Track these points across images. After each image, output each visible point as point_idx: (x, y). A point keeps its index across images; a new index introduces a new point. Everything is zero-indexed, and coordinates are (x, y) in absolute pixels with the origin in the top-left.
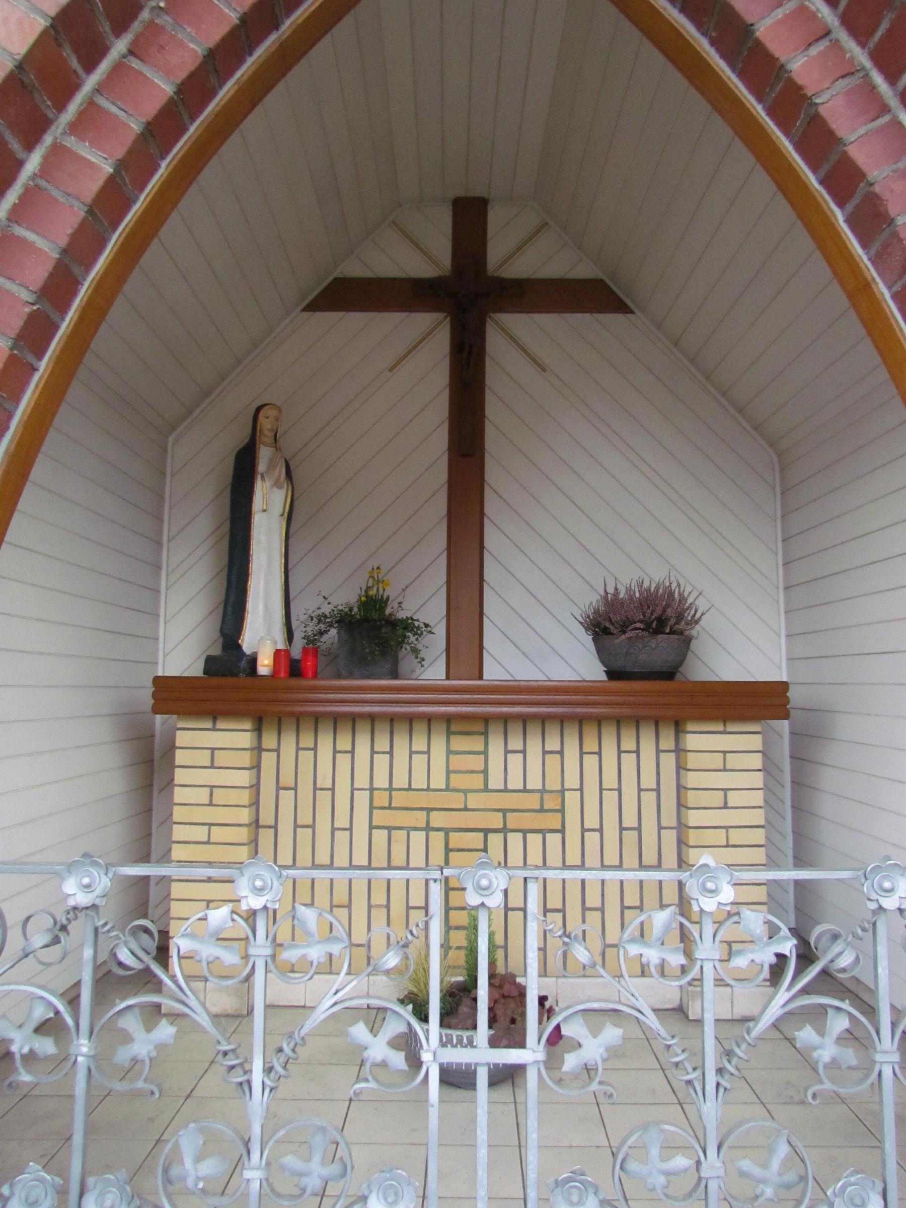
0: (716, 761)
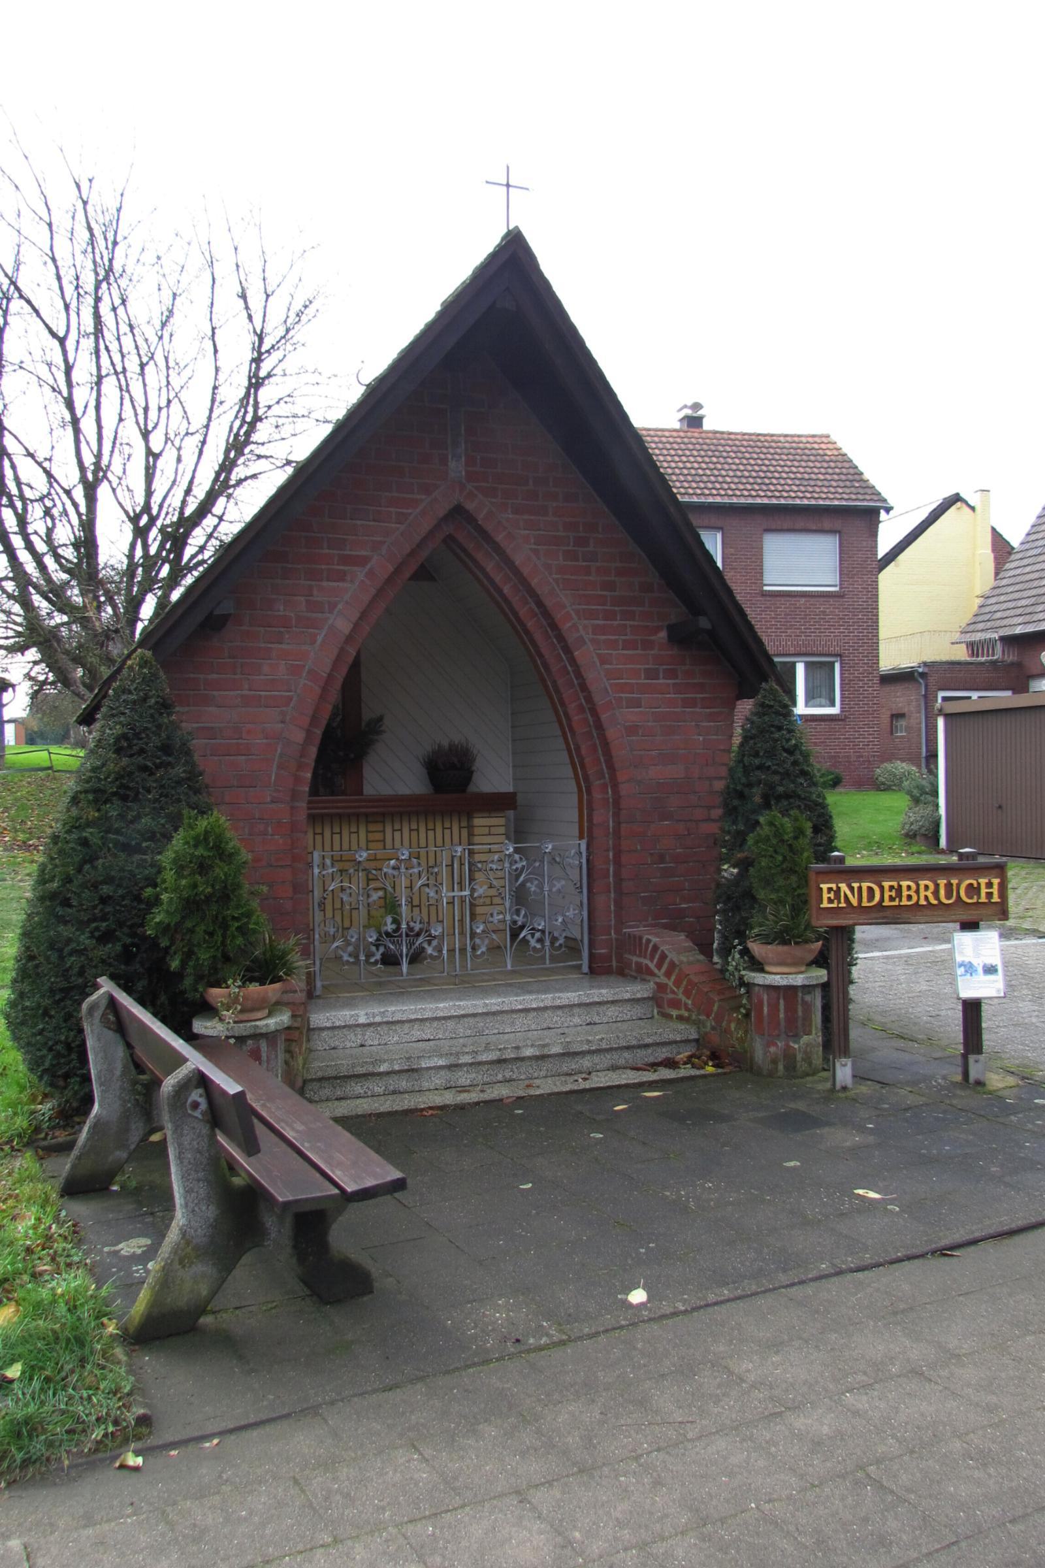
0: (486, 830)
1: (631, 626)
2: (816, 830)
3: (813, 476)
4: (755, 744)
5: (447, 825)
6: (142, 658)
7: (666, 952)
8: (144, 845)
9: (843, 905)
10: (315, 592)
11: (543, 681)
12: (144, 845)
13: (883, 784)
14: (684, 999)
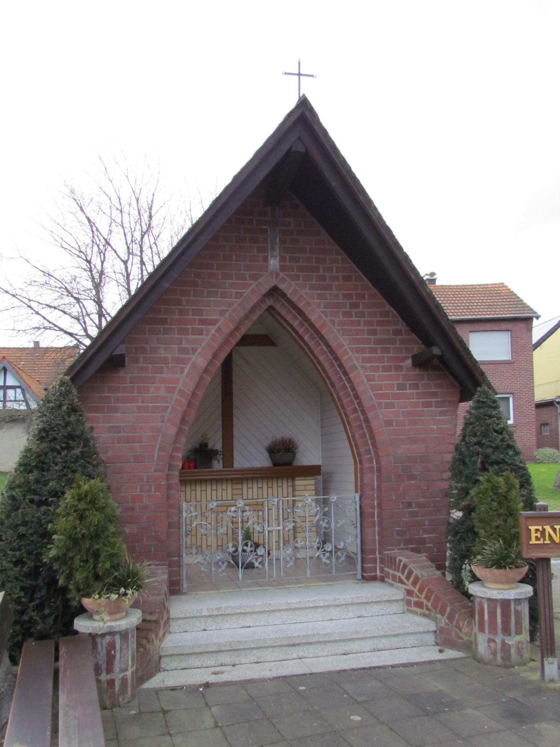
0: (303, 488)
1: (387, 357)
2: (522, 486)
3: (495, 304)
4: (474, 428)
5: (280, 484)
6: (61, 381)
7: (413, 569)
8: (50, 499)
9: (547, 542)
10: (184, 342)
11: (331, 394)
12: (50, 499)
13: (539, 460)
14: (425, 602)
